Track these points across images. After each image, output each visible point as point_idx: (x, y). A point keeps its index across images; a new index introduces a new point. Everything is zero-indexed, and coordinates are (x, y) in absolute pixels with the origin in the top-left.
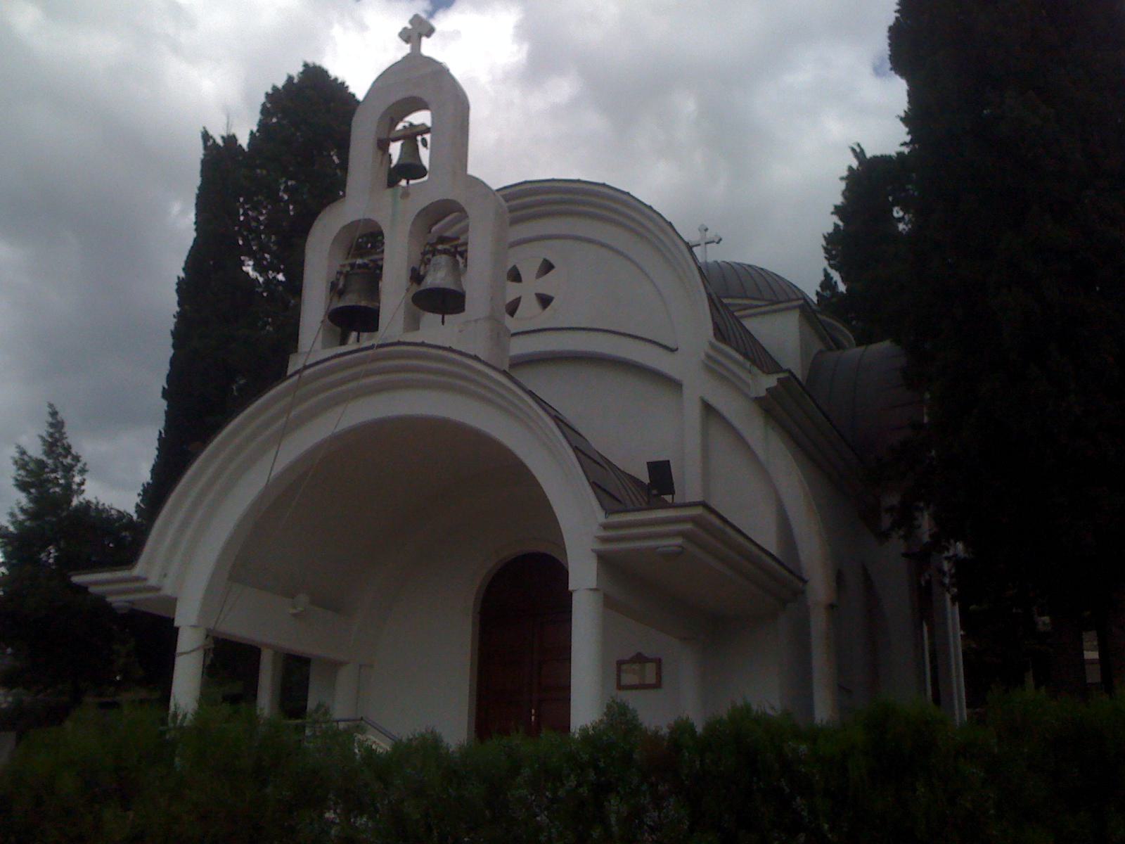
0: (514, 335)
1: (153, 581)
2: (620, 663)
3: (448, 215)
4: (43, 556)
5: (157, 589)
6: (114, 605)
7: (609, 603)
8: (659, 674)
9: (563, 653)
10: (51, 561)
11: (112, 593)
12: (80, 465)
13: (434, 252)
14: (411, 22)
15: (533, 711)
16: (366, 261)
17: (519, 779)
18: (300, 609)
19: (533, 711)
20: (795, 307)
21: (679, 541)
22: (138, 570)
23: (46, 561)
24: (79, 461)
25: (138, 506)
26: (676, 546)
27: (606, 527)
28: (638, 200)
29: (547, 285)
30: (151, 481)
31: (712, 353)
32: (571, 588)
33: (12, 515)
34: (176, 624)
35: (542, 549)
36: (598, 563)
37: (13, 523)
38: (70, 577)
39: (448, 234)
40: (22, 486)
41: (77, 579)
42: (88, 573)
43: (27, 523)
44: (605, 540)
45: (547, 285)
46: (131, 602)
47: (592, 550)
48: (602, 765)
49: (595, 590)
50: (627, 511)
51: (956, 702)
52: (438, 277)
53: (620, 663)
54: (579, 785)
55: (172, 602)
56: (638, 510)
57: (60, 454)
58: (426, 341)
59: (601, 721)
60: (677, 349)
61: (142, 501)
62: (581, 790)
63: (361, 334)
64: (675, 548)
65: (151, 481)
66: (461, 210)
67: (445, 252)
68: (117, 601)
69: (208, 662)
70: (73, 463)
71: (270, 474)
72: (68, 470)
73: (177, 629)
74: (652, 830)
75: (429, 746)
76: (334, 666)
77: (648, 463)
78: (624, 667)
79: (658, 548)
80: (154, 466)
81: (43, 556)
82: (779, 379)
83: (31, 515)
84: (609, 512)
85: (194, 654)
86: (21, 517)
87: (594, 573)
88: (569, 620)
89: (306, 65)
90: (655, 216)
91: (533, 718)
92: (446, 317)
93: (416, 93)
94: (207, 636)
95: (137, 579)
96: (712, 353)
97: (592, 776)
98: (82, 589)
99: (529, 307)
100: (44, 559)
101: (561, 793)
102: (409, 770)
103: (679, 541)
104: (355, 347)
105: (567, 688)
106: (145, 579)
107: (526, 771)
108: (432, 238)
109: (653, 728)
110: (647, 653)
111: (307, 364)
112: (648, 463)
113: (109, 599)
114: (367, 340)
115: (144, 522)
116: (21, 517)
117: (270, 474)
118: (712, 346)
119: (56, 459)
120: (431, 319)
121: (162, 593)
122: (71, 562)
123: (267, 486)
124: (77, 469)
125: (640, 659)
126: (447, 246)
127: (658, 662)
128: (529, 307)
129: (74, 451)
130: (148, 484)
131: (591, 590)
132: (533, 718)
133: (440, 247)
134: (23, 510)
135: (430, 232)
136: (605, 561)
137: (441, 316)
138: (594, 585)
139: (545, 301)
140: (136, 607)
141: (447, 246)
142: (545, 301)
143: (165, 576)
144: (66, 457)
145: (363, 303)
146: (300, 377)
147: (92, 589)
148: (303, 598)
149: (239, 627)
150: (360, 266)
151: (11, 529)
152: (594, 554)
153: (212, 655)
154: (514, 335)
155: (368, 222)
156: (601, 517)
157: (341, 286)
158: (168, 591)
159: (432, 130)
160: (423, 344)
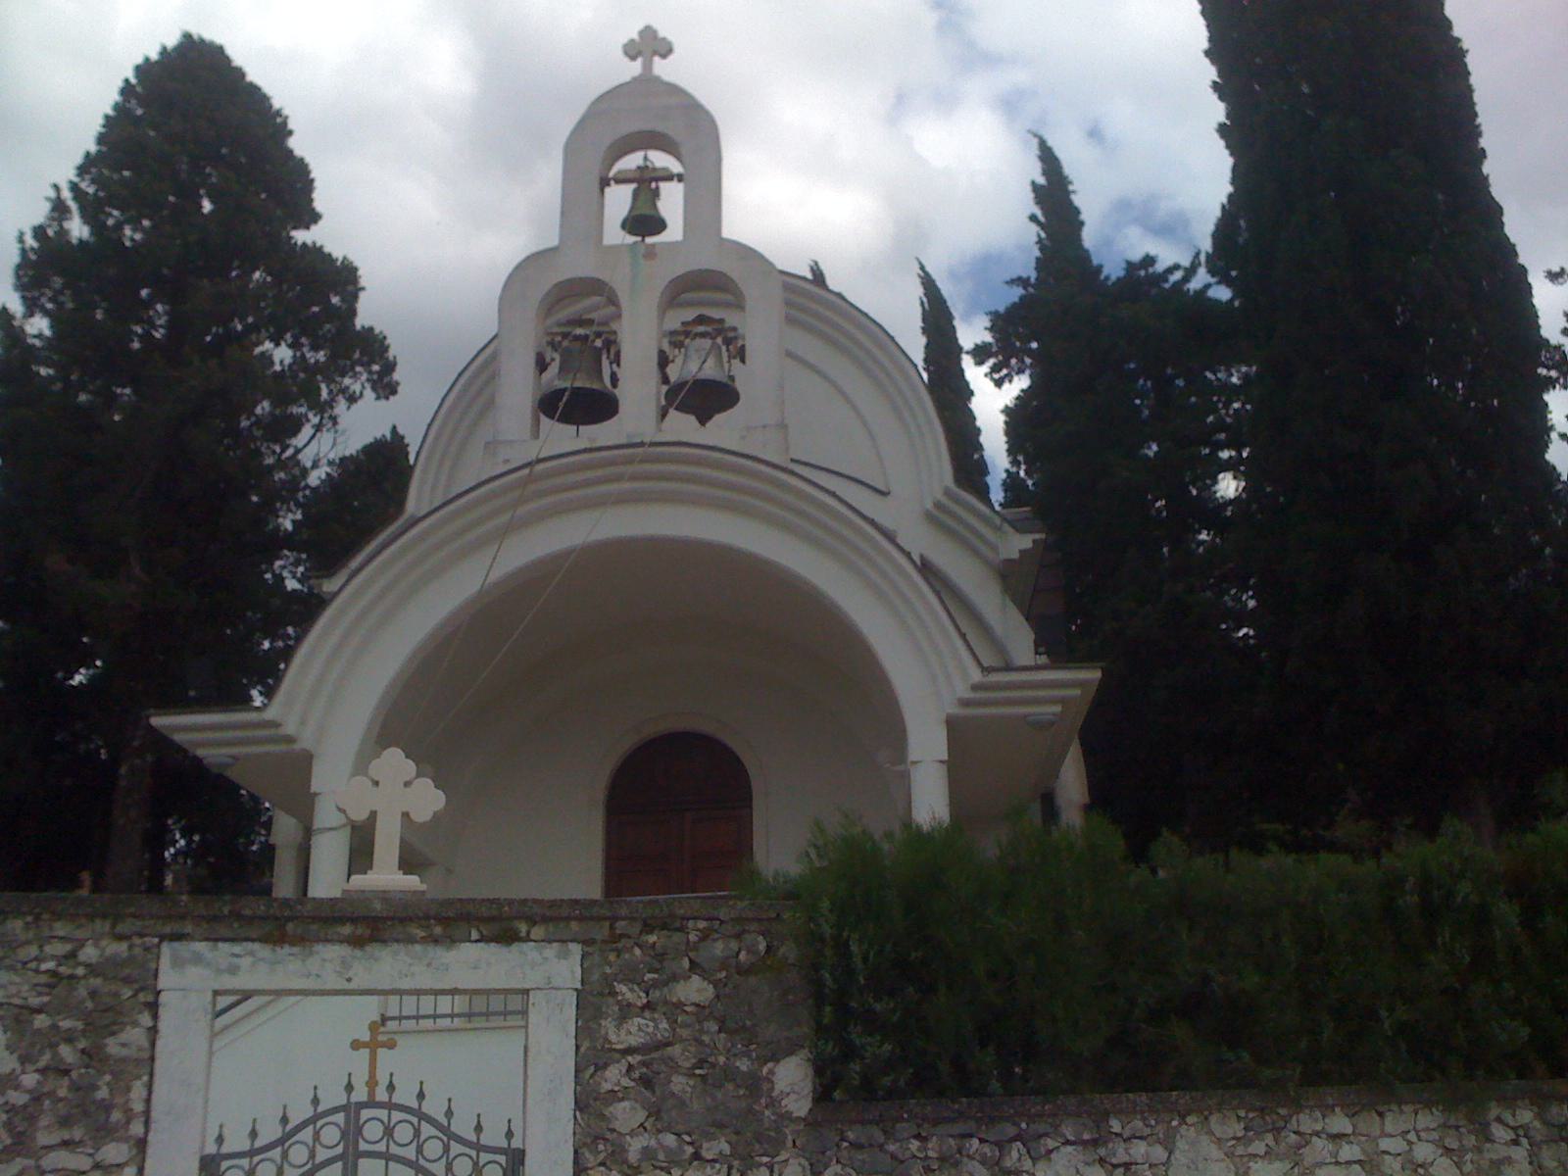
1: (290, 729)
5: (290, 740)
14: (641, 33)
21: (1057, 709)
26: (1054, 714)
28: (857, 308)
31: (945, 500)
38: (148, 717)
39: (593, 316)
41: (157, 721)
42: (204, 712)
52: (695, 364)
60: (889, 493)
64: (1051, 717)
82: (1034, 541)
89: (1467, 51)
90: (873, 327)
92: (581, 427)
93: (660, 127)
96: (945, 500)
103: (1057, 709)
111: (542, 456)
118: (947, 493)
121: (296, 747)
145: (588, 386)
146: (531, 472)
150: (577, 338)
158: (306, 742)
159: (685, 177)
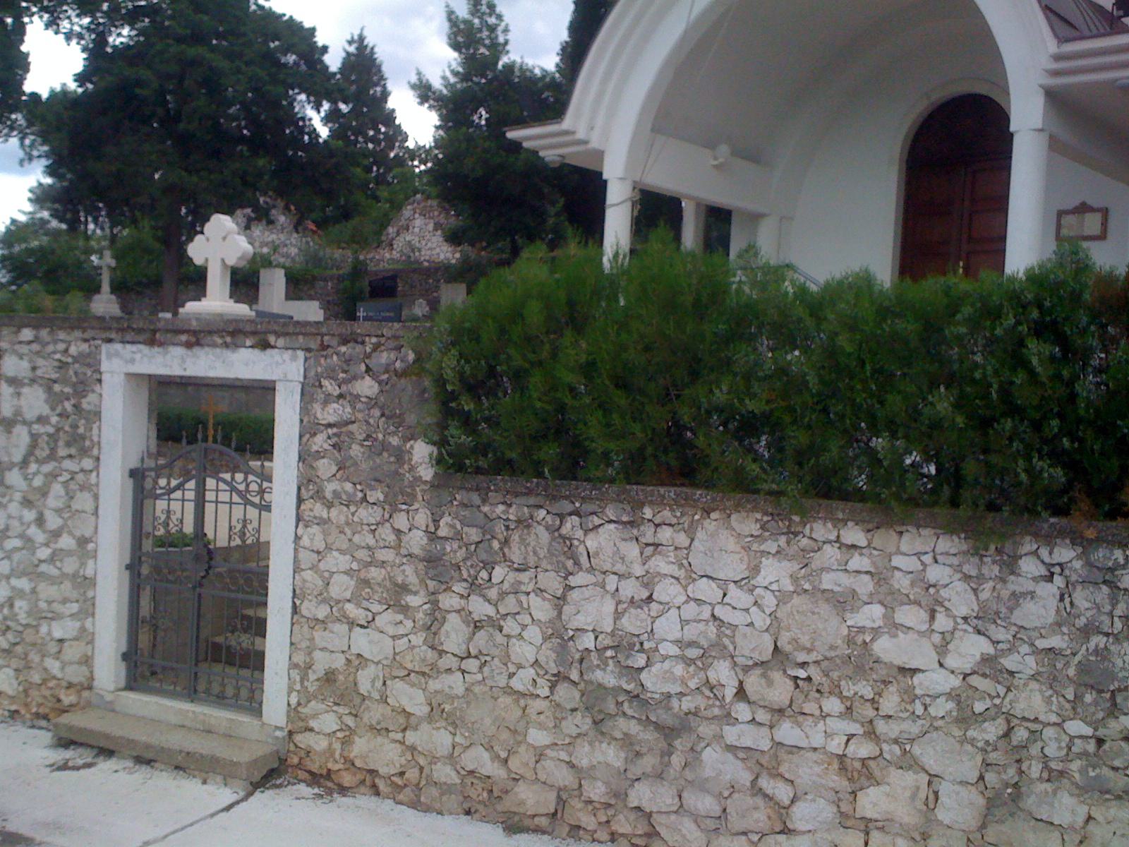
1: (581, 135)
2: (1061, 214)
4: (475, 118)
5: (586, 142)
6: (546, 159)
7: (1054, 145)
8: (1104, 224)
9: (1000, 203)
10: (483, 122)
11: (545, 148)
12: (503, 24)
18: (721, 160)
19: (961, 264)
22: (567, 123)
24: (502, 20)
25: (557, 65)
27: (1058, 58)
30: (568, 39)
32: (1012, 129)
33: (444, 78)
34: (605, 176)
35: (982, 89)
36: (1046, 102)
37: (446, 87)
40: (456, 46)
41: (512, 135)
43: (459, 86)
44: (1056, 73)
46: (562, 156)
47: (1041, 86)
48: (1047, 304)
49: (1041, 130)
50: (1082, 38)
53: (1061, 214)
54: (1018, 323)
55: (599, 155)
56: (1104, 35)
57: (483, 14)
59: (1049, 260)
61: (561, 60)
62: (1020, 328)
63: (139, 465)
65: (568, 39)
68: (550, 155)
69: (636, 213)
70: (498, 22)
71: (690, 14)
72: (492, 29)
73: (606, 182)
74: (1099, 371)
75: (862, 284)
76: (755, 218)
79: (1117, 80)
80: (571, 22)
81: (475, 118)
83: (465, 77)
84: (1062, 40)
85: (625, 204)
86: (452, 80)
87: (1041, 111)
88: (1008, 168)
94: (634, 188)
95: (567, 133)
97: (1035, 314)
98: (516, 146)
100: (477, 121)
101: (999, 331)
102: (843, 306)
105: (1003, 239)
106: (573, 133)
107: (967, 310)
109: (1108, 268)
113: (541, 154)
115: (564, 82)
116: (452, 80)
117: (690, 14)
119: (481, 18)
122: (499, 123)
123: (686, 32)
124: (500, 29)
127: (1105, 212)
129: (498, 10)
130: (566, 42)
131: (1035, 130)
134: (455, 74)
136: (1054, 97)
138: (1040, 126)
140: (567, 161)
143: (592, 128)
144: (490, 15)
147: (526, 145)
148: (724, 149)
149: (663, 181)
151: (445, 92)
152: (1041, 91)
153: (639, 207)
156: (1052, 46)
158: (595, 144)
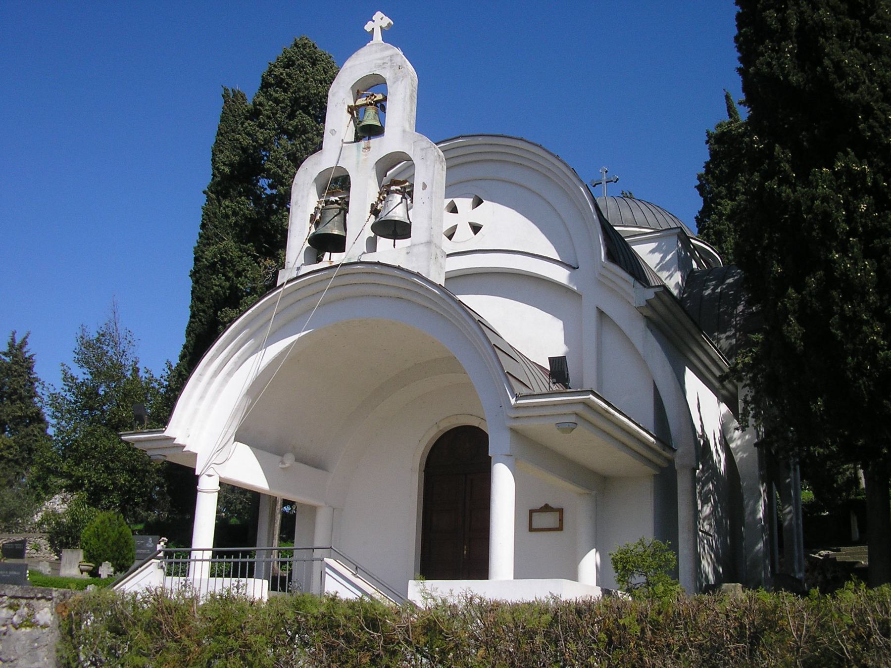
0: (449, 255)
2: (531, 512)
3: (401, 162)
13: (389, 192)
15: (465, 547)
16: (337, 198)
17: (712, 287)
19: (465, 547)
20: (673, 234)
23: (810, 175)
29: (450, 220)
45: (450, 220)
51: (796, 548)
58: (381, 262)
66: (410, 160)
67: (396, 192)
77: (549, 358)
78: (534, 514)
91: (465, 552)
99: (464, 233)
104: (328, 265)
108: (386, 181)
110: (552, 504)
112: (549, 358)
114: (337, 258)
120: (384, 243)
125: (546, 508)
126: (399, 188)
128: (464, 233)
132: (465, 552)
133: (393, 188)
135: (386, 176)
137: (393, 240)
139: (476, 228)
141: (399, 188)
142: (476, 228)
154: (449, 255)
155: (338, 168)
157: (318, 218)
160: (378, 263)
